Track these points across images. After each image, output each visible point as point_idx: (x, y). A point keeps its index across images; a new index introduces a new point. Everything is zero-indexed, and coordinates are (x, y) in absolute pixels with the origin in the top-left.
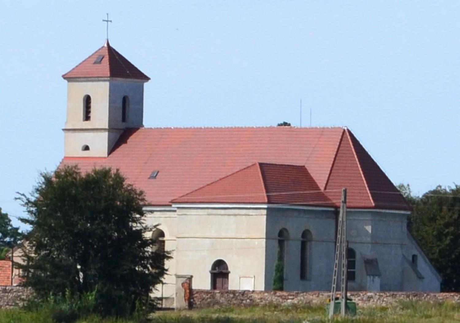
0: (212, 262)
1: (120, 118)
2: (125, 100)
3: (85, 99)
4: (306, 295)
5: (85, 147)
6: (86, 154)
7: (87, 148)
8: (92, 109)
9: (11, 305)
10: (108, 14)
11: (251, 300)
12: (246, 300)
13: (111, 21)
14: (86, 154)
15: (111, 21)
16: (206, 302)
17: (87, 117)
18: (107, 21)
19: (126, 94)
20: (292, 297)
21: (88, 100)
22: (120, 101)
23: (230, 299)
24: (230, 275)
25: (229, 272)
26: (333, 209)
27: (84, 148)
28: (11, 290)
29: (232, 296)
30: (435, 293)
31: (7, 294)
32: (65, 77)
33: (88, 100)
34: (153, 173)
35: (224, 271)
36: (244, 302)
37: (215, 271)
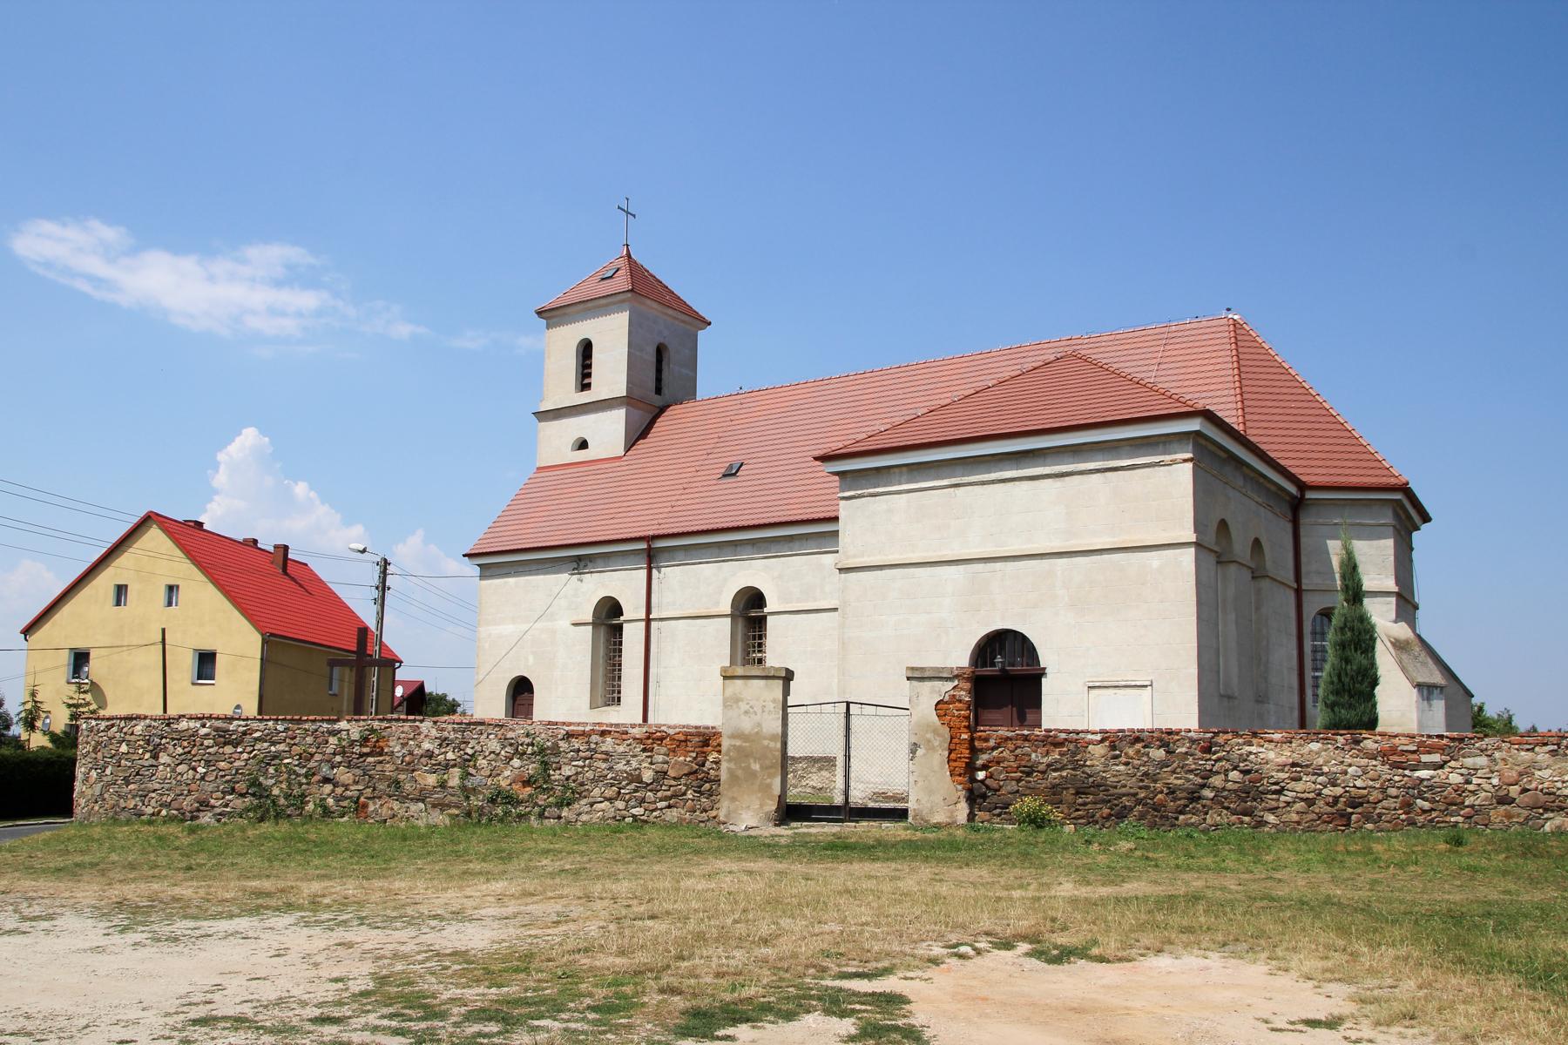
0: (972, 641)
1: (652, 384)
2: (660, 351)
3: (581, 350)
4: (1499, 749)
5: (581, 441)
6: (582, 455)
7: (583, 445)
8: (595, 370)
9: (243, 795)
10: (628, 199)
11: (1245, 772)
12: (1226, 772)
13: (634, 216)
14: (582, 455)
15: (634, 216)
16: (1044, 784)
17: (585, 387)
18: (648, 621)
19: (662, 341)
20: (1436, 758)
21: (586, 350)
22: (652, 350)
23: (1151, 770)
24: (1046, 683)
25: (1042, 673)
26: (1293, 489)
27: (579, 443)
28: (244, 733)
29: (1159, 754)
30: (60, 756)
31: (228, 749)
32: (540, 313)
33: (586, 350)
34: (731, 466)
35: (1019, 668)
36: (1217, 781)
37: (988, 671)
